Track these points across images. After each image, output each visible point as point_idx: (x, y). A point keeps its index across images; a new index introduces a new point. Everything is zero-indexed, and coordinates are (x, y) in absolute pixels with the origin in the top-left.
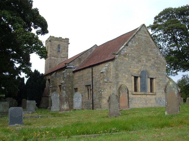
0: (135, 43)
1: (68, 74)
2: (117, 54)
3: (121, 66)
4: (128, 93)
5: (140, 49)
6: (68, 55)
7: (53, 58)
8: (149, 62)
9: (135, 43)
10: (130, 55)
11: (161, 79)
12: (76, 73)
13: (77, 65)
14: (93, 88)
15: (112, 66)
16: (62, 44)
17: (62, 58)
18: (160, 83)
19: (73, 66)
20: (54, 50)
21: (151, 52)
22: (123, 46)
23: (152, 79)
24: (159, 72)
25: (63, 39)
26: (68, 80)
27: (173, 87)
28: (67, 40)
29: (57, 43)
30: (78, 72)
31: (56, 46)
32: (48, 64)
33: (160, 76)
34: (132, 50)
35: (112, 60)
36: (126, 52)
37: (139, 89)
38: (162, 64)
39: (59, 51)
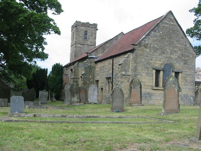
0: (159, 32)
1: (89, 64)
2: (136, 45)
4: (141, 87)
6: (95, 42)
7: (79, 45)
8: (175, 54)
9: (159, 32)
10: (152, 45)
11: (188, 73)
12: (98, 64)
13: (100, 55)
14: (113, 81)
15: (131, 57)
16: (90, 30)
17: (89, 46)
18: (188, 78)
20: (80, 37)
22: (145, 36)
23: (177, 74)
26: (90, 71)
28: (170, 13)
29: (84, 28)
30: (100, 63)
31: (83, 32)
32: (73, 52)
33: (187, 70)
34: (154, 40)
35: (132, 51)
36: (147, 42)
37: (161, 84)
39: (86, 38)
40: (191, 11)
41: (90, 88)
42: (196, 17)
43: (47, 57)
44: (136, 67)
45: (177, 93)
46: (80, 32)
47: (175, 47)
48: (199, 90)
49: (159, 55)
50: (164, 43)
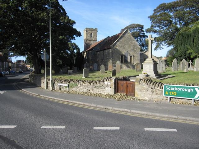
1: (94, 53)
6: (97, 38)
16: (93, 32)
29: (90, 32)
39: (91, 37)
41: (95, 64)
42: (147, 24)
43: (80, 36)
44: (112, 55)
47: (160, 31)
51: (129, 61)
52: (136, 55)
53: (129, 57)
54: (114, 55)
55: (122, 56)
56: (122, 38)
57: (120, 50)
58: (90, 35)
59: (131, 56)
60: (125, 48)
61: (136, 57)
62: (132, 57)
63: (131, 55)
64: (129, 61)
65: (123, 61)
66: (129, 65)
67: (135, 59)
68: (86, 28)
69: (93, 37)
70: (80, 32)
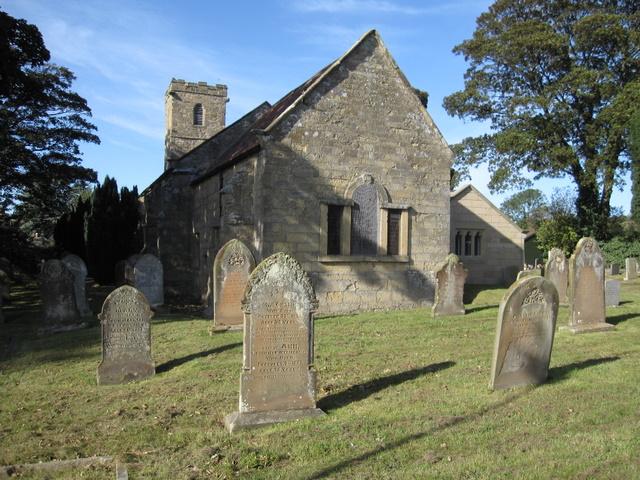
1: (176, 191)
2: (266, 134)
3: (280, 172)
5: (356, 114)
8: (388, 156)
10: (316, 134)
13: (207, 165)
19: (195, 167)
21: (395, 124)
22: (292, 106)
24: (423, 190)
25: (209, 88)
27: (288, 287)
29: (193, 99)
33: (425, 203)
38: (435, 162)
39: (197, 122)
40: (456, 50)
45: (303, 327)
46: (184, 107)
48: (449, 268)
49: (340, 161)
50: (355, 125)
51: (382, 240)
52: (425, 206)
53: (382, 217)
54: (276, 202)
55: (335, 210)
56: (333, 85)
57: (321, 167)
58: (189, 115)
59: (398, 211)
60: (354, 155)
61: (430, 216)
62: (404, 218)
63: (394, 205)
64: (382, 240)
65: (346, 246)
66: (380, 270)
67: (423, 232)
68: (174, 81)
69: (207, 124)
70: (35, 27)
